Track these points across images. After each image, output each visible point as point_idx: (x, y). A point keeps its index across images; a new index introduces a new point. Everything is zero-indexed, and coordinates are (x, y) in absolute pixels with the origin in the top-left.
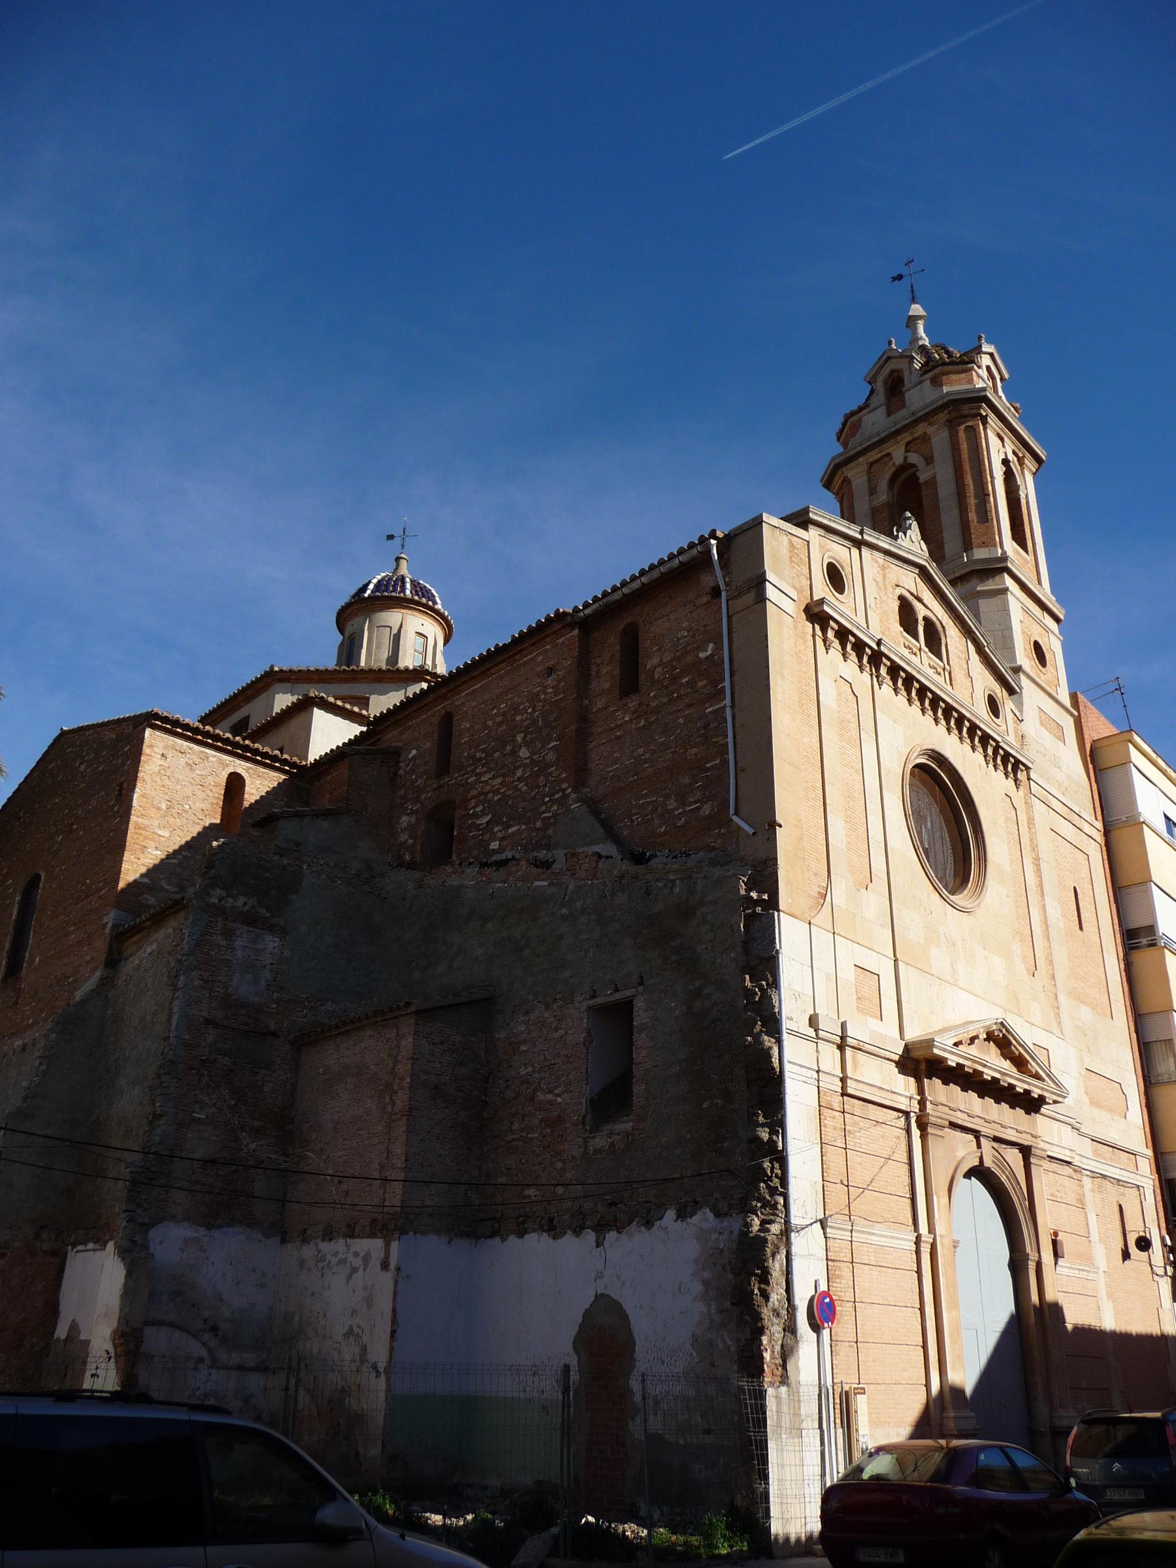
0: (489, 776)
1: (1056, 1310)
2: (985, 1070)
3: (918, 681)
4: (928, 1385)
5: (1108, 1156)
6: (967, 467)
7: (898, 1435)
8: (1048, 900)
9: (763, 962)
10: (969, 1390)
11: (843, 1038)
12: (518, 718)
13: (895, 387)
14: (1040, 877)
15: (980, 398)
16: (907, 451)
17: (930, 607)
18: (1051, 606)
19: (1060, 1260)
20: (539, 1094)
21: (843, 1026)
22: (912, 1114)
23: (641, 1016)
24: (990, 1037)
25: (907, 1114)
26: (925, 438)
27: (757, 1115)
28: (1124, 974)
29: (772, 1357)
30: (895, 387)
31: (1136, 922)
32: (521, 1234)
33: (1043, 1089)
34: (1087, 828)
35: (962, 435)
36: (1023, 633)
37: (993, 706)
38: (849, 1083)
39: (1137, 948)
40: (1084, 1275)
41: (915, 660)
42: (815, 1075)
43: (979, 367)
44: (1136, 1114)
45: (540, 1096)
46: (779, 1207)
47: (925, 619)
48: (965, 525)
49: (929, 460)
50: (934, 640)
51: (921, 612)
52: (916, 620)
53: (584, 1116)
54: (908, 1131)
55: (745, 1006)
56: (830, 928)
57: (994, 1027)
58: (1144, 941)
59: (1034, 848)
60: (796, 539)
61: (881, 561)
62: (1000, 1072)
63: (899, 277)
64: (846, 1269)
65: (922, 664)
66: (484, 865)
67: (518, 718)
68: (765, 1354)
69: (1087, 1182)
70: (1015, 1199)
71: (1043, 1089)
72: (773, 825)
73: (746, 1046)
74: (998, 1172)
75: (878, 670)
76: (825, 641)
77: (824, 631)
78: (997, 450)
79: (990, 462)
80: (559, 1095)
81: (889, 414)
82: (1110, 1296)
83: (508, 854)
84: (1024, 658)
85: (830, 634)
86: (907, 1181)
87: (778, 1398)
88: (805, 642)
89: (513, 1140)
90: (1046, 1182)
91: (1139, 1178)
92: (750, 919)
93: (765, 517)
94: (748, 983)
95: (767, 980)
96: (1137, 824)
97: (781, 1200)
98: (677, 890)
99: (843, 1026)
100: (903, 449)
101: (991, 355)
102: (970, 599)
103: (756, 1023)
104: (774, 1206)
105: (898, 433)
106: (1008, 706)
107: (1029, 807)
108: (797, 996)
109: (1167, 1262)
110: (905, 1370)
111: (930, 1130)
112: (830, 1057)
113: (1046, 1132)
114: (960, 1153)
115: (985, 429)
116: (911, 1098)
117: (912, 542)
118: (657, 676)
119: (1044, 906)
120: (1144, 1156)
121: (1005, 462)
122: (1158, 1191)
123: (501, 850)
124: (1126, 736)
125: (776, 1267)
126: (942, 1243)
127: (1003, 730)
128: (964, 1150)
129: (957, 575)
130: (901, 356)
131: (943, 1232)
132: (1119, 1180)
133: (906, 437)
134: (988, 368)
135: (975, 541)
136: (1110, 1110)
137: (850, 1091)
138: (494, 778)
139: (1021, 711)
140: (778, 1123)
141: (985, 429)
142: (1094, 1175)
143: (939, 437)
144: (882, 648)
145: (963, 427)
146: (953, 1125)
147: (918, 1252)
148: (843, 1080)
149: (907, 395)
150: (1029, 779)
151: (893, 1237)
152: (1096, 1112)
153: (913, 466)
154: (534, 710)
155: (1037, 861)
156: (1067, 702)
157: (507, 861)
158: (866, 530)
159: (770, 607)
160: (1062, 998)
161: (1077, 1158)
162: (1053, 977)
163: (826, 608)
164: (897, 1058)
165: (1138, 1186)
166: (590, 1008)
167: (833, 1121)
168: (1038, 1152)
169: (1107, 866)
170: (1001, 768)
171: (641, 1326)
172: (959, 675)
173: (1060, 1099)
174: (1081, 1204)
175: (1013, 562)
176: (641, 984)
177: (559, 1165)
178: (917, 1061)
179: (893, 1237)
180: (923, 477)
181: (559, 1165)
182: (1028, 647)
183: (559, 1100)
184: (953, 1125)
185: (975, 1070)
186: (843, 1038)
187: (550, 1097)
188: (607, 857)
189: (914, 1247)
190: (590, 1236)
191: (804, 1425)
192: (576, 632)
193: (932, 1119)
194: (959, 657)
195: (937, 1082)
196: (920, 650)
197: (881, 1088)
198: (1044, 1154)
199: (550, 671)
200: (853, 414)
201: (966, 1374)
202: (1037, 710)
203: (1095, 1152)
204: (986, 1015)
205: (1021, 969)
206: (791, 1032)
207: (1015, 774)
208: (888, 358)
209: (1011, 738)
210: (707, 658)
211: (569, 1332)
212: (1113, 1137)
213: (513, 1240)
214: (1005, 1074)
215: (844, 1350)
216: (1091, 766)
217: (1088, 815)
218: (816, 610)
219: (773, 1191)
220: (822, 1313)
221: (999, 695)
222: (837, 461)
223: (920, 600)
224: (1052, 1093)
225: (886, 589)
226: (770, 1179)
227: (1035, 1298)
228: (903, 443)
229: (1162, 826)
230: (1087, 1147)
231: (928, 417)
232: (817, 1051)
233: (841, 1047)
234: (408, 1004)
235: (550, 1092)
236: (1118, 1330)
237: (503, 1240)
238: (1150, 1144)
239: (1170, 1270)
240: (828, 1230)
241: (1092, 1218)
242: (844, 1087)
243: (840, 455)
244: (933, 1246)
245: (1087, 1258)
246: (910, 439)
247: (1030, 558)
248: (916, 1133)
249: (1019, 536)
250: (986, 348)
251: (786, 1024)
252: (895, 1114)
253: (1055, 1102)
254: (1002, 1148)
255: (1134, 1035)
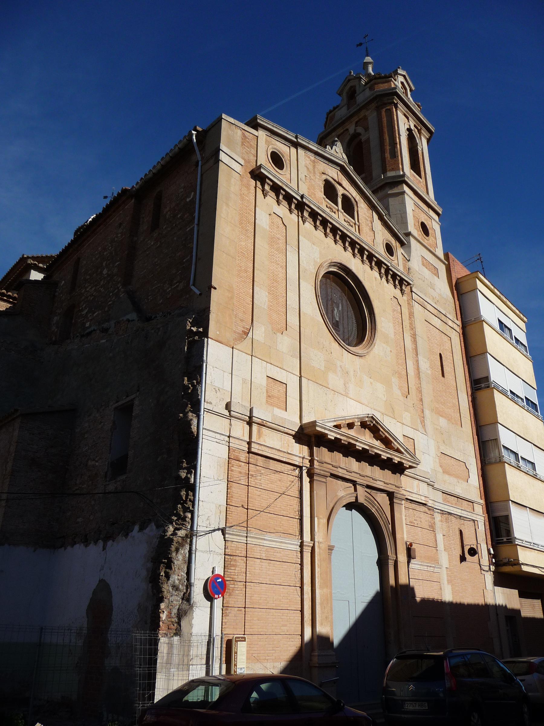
0: (90, 287)
1: (409, 590)
2: (357, 444)
3: (331, 223)
4: (302, 635)
5: (454, 502)
6: (386, 130)
7: (274, 667)
8: (420, 358)
9: (194, 367)
10: (336, 640)
11: (251, 417)
12: (105, 253)
13: (352, 95)
14: (416, 345)
15: (394, 93)
16: (356, 126)
17: (346, 188)
18: (433, 205)
19: (412, 561)
20: (89, 462)
21: (251, 411)
22: (304, 468)
23: (136, 411)
24: (364, 425)
25: (301, 468)
26: (365, 118)
27: (183, 462)
28: (471, 403)
29: (169, 616)
30: (352, 95)
31: (479, 375)
32: (73, 544)
33: (401, 458)
34: (450, 323)
35: (383, 113)
36: (414, 216)
37: (389, 249)
38: (253, 445)
39: (480, 389)
40: (429, 569)
41: (335, 216)
42: (227, 439)
43: (395, 80)
44: (475, 479)
45: (90, 463)
46: (187, 519)
47: (344, 196)
48: (383, 160)
49: (366, 129)
50: (349, 207)
51: (340, 191)
52: (337, 195)
53: (106, 473)
54: (301, 478)
55: (183, 395)
56: (250, 353)
57: (367, 419)
58: (483, 385)
59: (412, 328)
60: (248, 134)
61: (313, 158)
62: (369, 446)
63: (361, 44)
64: (240, 562)
65: (339, 218)
66: (82, 336)
67: (105, 253)
68: (161, 615)
69: (438, 517)
70: (381, 523)
71: (401, 458)
72: (210, 287)
73: (179, 420)
74: (370, 506)
75: (302, 213)
76: (263, 190)
77: (263, 185)
78: (403, 124)
79: (398, 127)
80: (97, 462)
81: (348, 109)
82: (449, 582)
83: (92, 328)
84: (413, 228)
85: (267, 187)
86: (297, 508)
87: (170, 645)
88: (248, 189)
89: (76, 490)
90: (404, 515)
91: (474, 515)
92: (192, 344)
93: (224, 116)
94: (186, 382)
95: (197, 380)
96: (480, 321)
97: (189, 515)
98: (160, 333)
99: (251, 411)
100: (354, 126)
101: (404, 76)
102: (384, 200)
103: (187, 406)
104: (184, 519)
105: (351, 116)
106: (399, 251)
107: (410, 306)
108: (217, 390)
109: (491, 563)
110: (285, 626)
111: (315, 478)
112: (240, 430)
113: (407, 485)
114: (341, 494)
115: (396, 111)
116: (303, 458)
117: (337, 151)
118: (167, 217)
119: (417, 361)
120: (479, 504)
121: (409, 130)
122: (487, 523)
123: (90, 326)
124: (475, 275)
125: (179, 559)
126: (319, 547)
127: (397, 263)
128: (345, 492)
129: (378, 186)
130: (355, 78)
131: (321, 540)
132: (460, 516)
133: (356, 119)
134: (402, 83)
135: (388, 168)
136: (458, 477)
137: (253, 450)
138: (91, 289)
139: (409, 256)
140: (193, 466)
141: (396, 111)
142: (443, 512)
143: (371, 116)
144: (304, 200)
145: (384, 110)
146: (334, 476)
147: (302, 552)
148: (249, 443)
149: (357, 98)
150: (412, 291)
151: (281, 542)
152: (447, 477)
153: (359, 134)
154: (112, 248)
155: (414, 337)
156: (442, 257)
157: (91, 332)
158: (299, 136)
159: (221, 166)
160: (427, 412)
161: (430, 502)
162: (421, 400)
163: (262, 170)
164: (294, 433)
165: (474, 521)
166: (116, 408)
167: (239, 469)
168: (399, 496)
169: (463, 345)
170: (399, 287)
171: (116, 600)
172: (365, 229)
173: (415, 465)
174: (432, 528)
175: (408, 178)
176: (138, 391)
177: (93, 503)
178: (309, 436)
179: (281, 542)
180: (363, 138)
181: (93, 503)
182: (417, 224)
183: (97, 464)
184: (334, 476)
185: (349, 443)
186: (251, 417)
187: (93, 463)
188: (132, 321)
189: (299, 549)
190: (101, 543)
191: (194, 662)
192: (133, 201)
193: (316, 471)
194: (366, 219)
195: (324, 450)
196: (338, 210)
197: (279, 450)
198: (404, 497)
199: (121, 224)
200: (331, 112)
201: (336, 627)
202: (420, 258)
203: (444, 500)
204: (355, 410)
205: (397, 392)
206: (209, 411)
207: (401, 287)
208: (348, 80)
209: (401, 268)
210: (190, 201)
211: (85, 603)
212: (458, 491)
213: (69, 548)
214: (372, 447)
215: (233, 612)
216: (455, 292)
217: (452, 316)
218: (257, 172)
219: (186, 510)
220: (215, 588)
221: (394, 244)
222: (321, 136)
223: (340, 185)
224: (408, 461)
225: (314, 173)
226: (185, 502)
227: (392, 582)
228: (354, 123)
229: (497, 326)
230: (439, 496)
231: (365, 106)
232: (231, 425)
233: (250, 423)
234: (16, 410)
235: (94, 460)
236: (454, 601)
237: (65, 549)
238: (483, 497)
239: (493, 568)
240: (227, 536)
241: (440, 537)
242: (249, 448)
243: (323, 133)
244: (313, 549)
245: (435, 560)
246: (358, 119)
247: (423, 181)
248: (306, 480)
249: (415, 166)
250: (400, 71)
251: (204, 405)
252: (292, 467)
253: (411, 467)
254: (373, 492)
255: (476, 437)
